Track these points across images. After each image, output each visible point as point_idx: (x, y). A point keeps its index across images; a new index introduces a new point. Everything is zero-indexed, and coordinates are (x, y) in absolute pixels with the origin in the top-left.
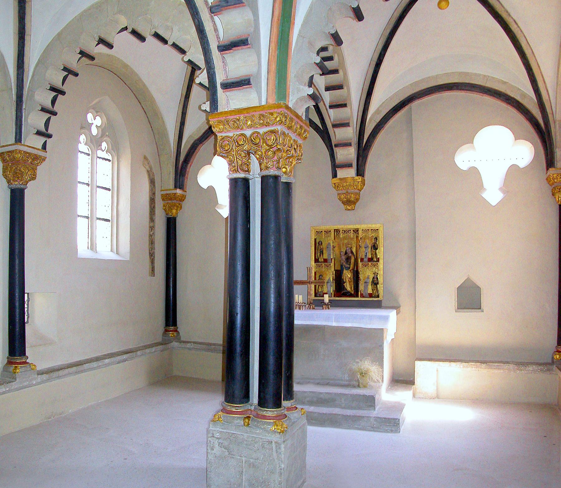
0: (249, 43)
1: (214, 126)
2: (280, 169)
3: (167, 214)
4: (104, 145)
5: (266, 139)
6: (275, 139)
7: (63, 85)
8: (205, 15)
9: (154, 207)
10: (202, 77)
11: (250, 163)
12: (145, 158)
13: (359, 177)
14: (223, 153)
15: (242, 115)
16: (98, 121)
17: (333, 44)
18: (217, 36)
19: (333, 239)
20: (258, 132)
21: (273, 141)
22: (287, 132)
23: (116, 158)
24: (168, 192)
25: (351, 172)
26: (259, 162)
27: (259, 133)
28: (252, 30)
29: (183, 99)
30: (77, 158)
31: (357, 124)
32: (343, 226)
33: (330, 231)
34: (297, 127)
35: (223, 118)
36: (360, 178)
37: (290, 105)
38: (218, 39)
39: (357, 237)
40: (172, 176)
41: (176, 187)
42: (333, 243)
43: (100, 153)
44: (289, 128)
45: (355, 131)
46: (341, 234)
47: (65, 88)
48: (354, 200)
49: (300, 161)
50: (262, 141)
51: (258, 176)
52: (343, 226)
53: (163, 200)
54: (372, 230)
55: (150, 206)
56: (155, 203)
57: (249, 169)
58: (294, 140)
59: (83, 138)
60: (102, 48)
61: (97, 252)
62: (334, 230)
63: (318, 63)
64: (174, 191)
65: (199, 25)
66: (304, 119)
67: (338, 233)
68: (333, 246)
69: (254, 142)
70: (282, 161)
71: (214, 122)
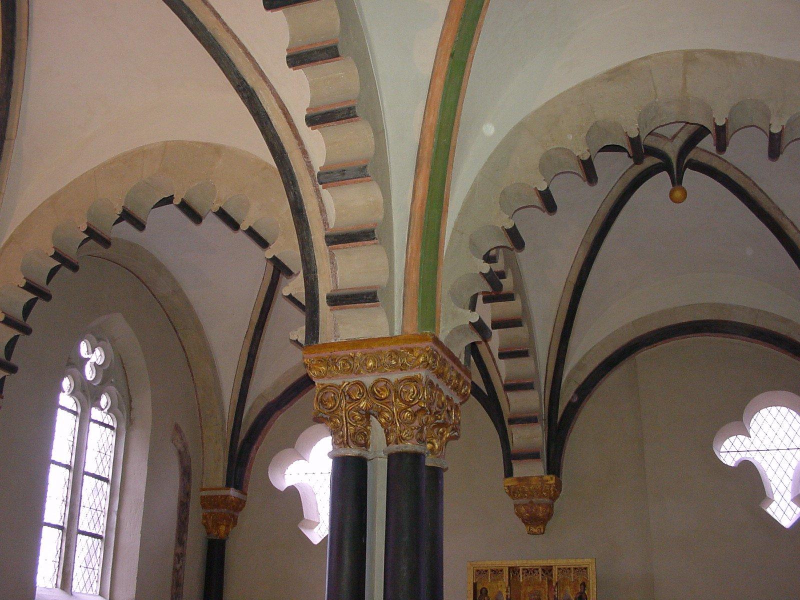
0: (376, 236)
1: (310, 367)
2: (424, 442)
3: (208, 534)
4: (104, 400)
5: (401, 392)
6: (416, 393)
7: (48, 283)
8: (306, 187)
9: (186, 518)
10: (295, 286)
11: (369, 431)
12: (177, 428)
13: (552, 476)
14: (325, 413)
15: (360, 351)
16: (98, 357)
17: (510, 246)
18: (323, 220)
19: (507, 584)
20: (387, 379)
21: (413, 395)
22: (435, 381)
23: (123, 426)
24: (213, 493)
25: (535, 469)
26: (385, 431)
27: (389, 381)
28: (381, 217)
29: (252, 331)
30: (54, 415)
31: (545, 386)
32: (525, 562)
33: (502, 570)
34: (451, 376)
35: (325, 354)
36: (554, 478)
37: (442, 338)
38: (325, 226)
39: (550, 582)
40: (223, 465)
41: (228, 485)
42: (507, 591)
43: (96, 414)
44: (440, 375)
45: (543, 398)
46: (521, 576)
47: (51, 288)
48: (543, 516)
49: (456, 433)
50: (393, 394)
51: (383, 455)
52: (525, 562)
53: (204, 507)
54: (575, 569)
55: (180, 517)
56: (188, 511)
57: (367, 443)
58: (447, 398)
59: (66, 383)
60: (126, 230)
61: (72, 594)
62: (510, 568)
63: (487, 274)
64: (224, 492)
65: (296, 202)
66: (463, 363)
67: (517, 574)
68: (507, 596)
69: (376, 395)
70: (427, 429)
71: (310, 360)
